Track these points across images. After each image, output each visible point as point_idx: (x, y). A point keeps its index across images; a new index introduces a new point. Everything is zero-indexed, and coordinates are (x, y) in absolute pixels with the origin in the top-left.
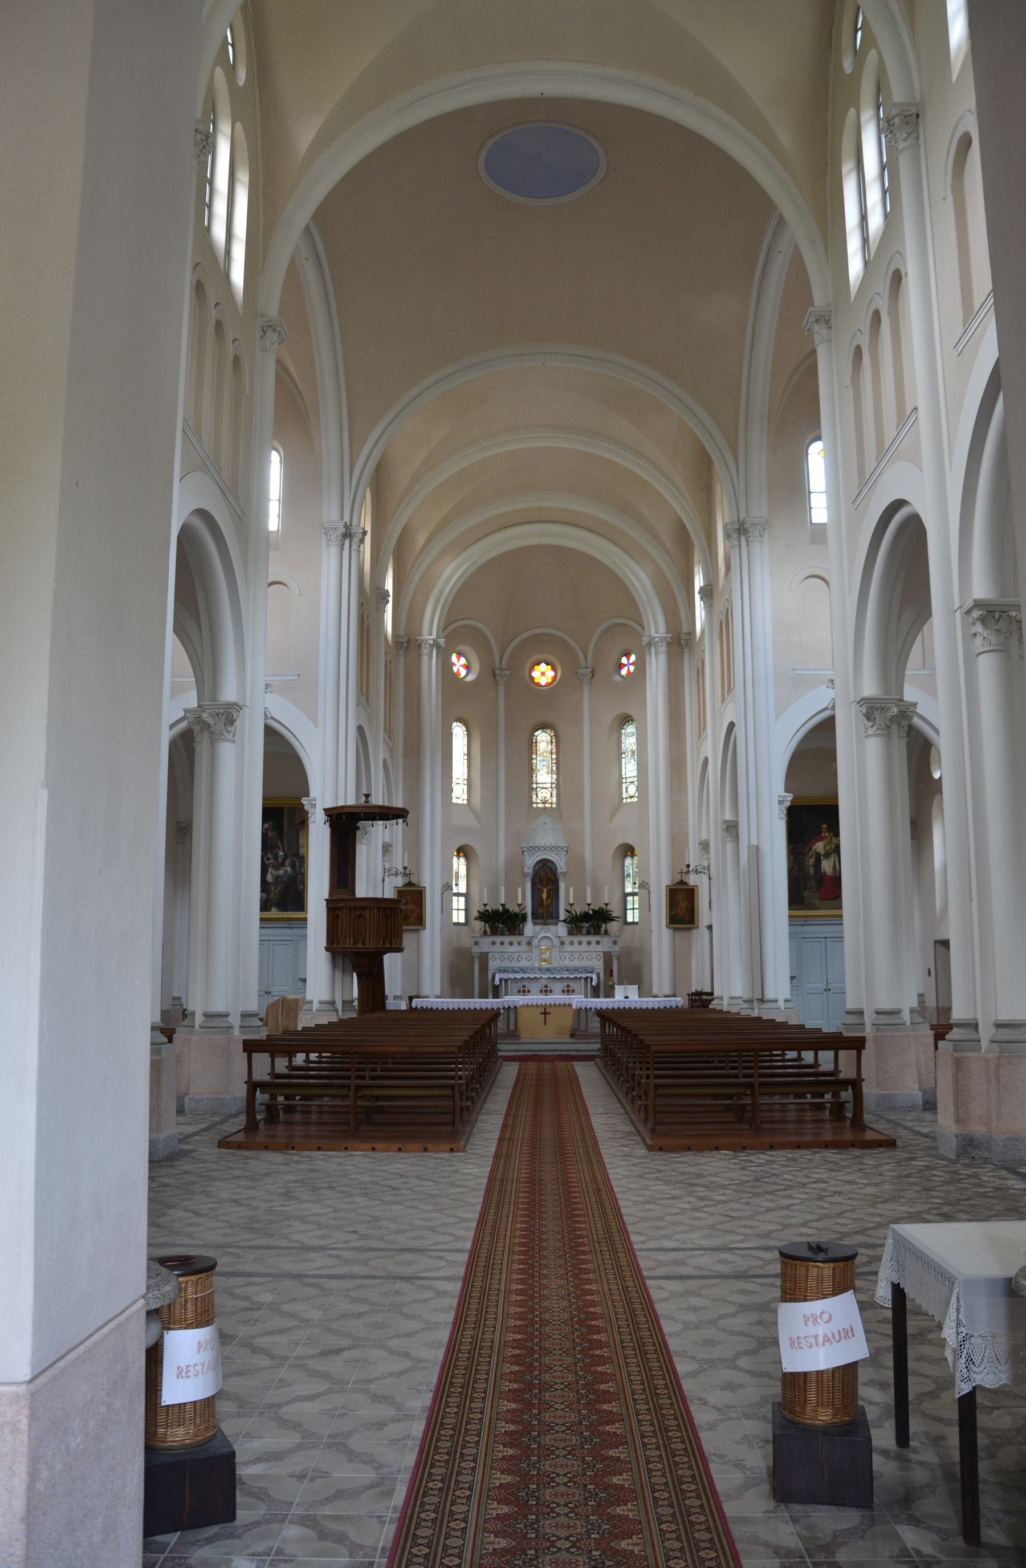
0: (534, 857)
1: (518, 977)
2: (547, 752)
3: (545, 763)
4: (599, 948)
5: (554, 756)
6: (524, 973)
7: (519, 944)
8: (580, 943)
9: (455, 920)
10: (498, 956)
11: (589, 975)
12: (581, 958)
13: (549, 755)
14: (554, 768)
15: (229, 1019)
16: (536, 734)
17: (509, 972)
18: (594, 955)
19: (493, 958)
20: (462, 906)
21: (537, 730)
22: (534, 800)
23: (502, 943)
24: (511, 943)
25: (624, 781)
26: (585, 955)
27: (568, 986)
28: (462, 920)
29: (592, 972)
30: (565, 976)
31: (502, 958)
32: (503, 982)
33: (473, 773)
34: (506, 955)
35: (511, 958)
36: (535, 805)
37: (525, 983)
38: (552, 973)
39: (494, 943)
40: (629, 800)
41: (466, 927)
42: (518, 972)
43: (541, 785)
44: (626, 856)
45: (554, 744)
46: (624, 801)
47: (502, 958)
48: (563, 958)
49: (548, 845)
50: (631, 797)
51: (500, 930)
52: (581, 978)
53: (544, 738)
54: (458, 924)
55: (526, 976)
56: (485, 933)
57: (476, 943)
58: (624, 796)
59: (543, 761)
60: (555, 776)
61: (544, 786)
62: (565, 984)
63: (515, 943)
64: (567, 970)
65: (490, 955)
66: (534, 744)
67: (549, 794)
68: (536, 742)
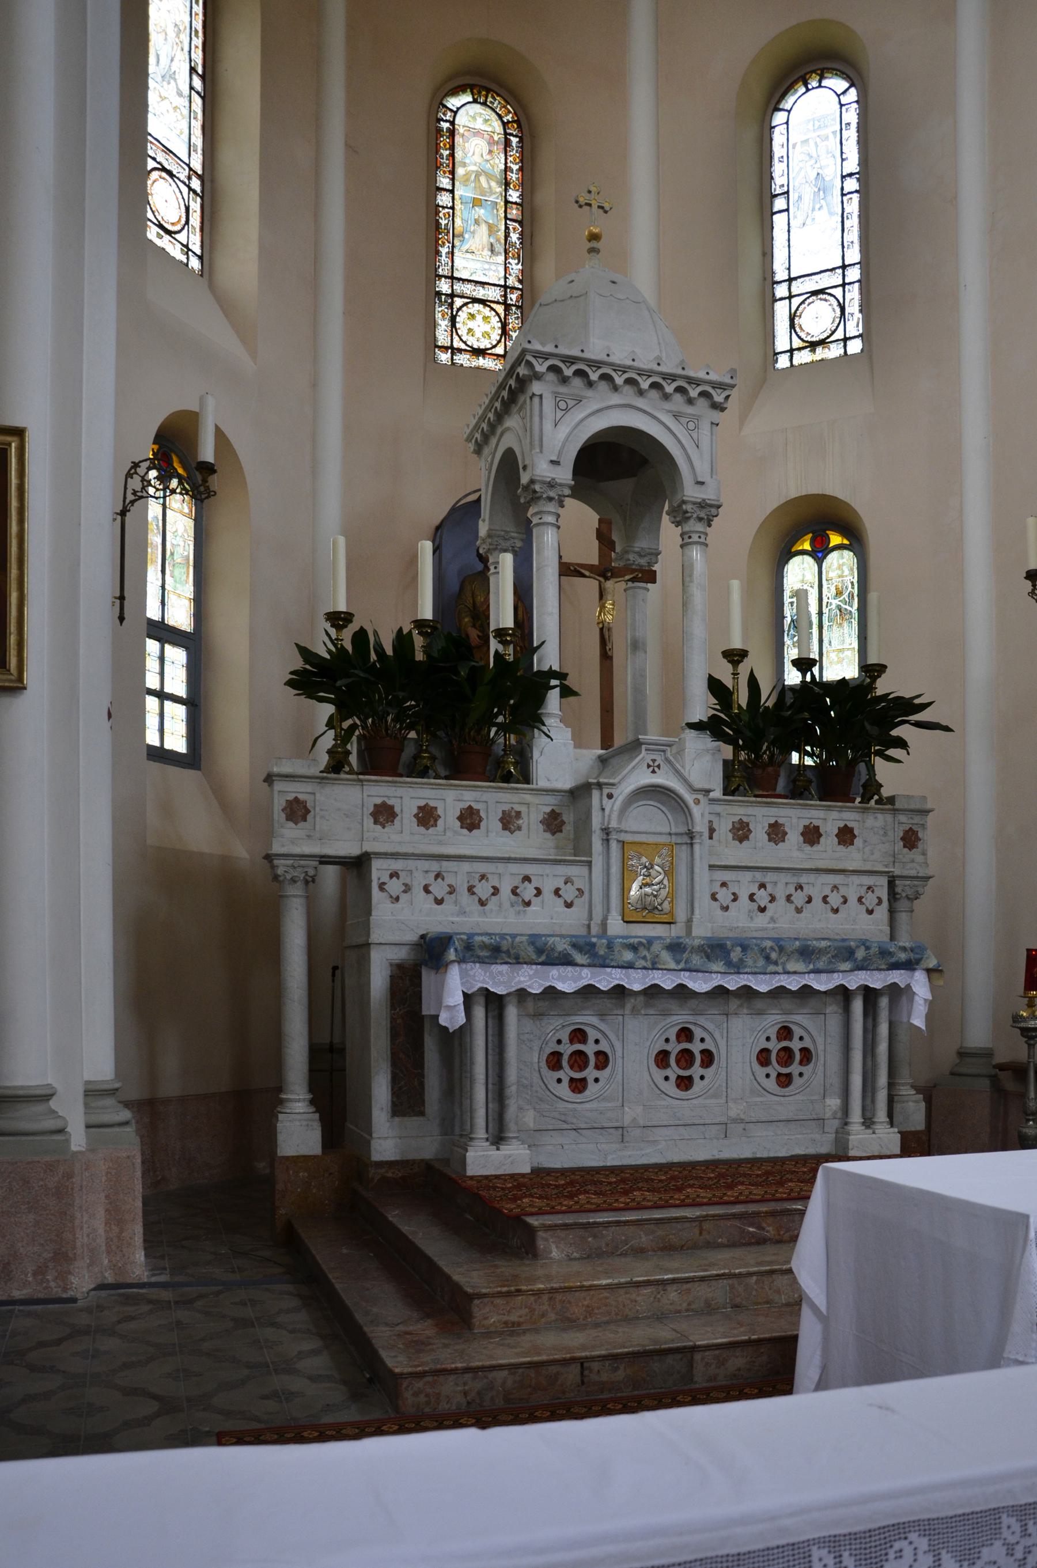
0: (579, 414)
1: (566, 987)
2: (489, 176)
3: (481, 212)
4: (852, 857)
5: (514, 196)
6: (600, 962)
7: (509, 821)
8: (776, 833)
9: (152, 738)
10: (420, 873)
11: (897, 977)
12: (799, 898)
13: (499, 189)
14: (514, 237)
15: (53, 1104)
16: (453, 102)
17: (518, 960)
18: (853, 887)
19: (395, 887)
20: (177, 683)
21: (455, 92)
22: (442, 337)
23: (427, 817)
24: (470, 819)
25: (781, 291)
26: (816, 887)
27: (785, 1032)
28: (177, 742)
29: (909, 966)
30: (793, 984)
31: (439, 889)
32: (479, 1012)
33: (227, 155)
34: (460, 874)
35: (483, 890)
36: (444, 357)
37: (586, 1019)
38: (737, 968)
39: (384, 814)
40: (803, 357)
41: (189, 775)
42: (566, 961)
43: (468, 289)
44: (787, 554)
45: (514, 153)
46: (783, 362)
47: (439, 889)
48: (724, 896)
49: (645, 362)
50: (813, 346)
51: (409, 751)
52: (843, 994)
53: (479, 124)
54: (160, 755)
55: (605, 980)
56: (337, 764)
57: (297, 811)
58: (782, 343)
59: (476, 203)
60: (516, 267)
61: (480, 293)
62: (772, 1021)
63: (491, 821)
64: (806, 953)
65: (379, 870)
66: (445, 140)
67: (484, 344)
68: (452, 133)
